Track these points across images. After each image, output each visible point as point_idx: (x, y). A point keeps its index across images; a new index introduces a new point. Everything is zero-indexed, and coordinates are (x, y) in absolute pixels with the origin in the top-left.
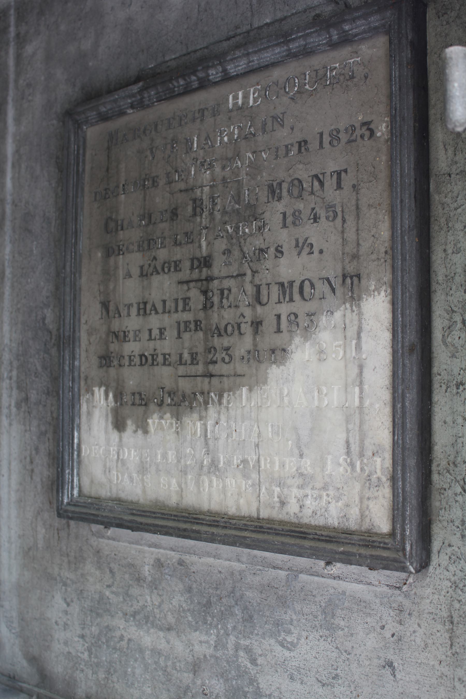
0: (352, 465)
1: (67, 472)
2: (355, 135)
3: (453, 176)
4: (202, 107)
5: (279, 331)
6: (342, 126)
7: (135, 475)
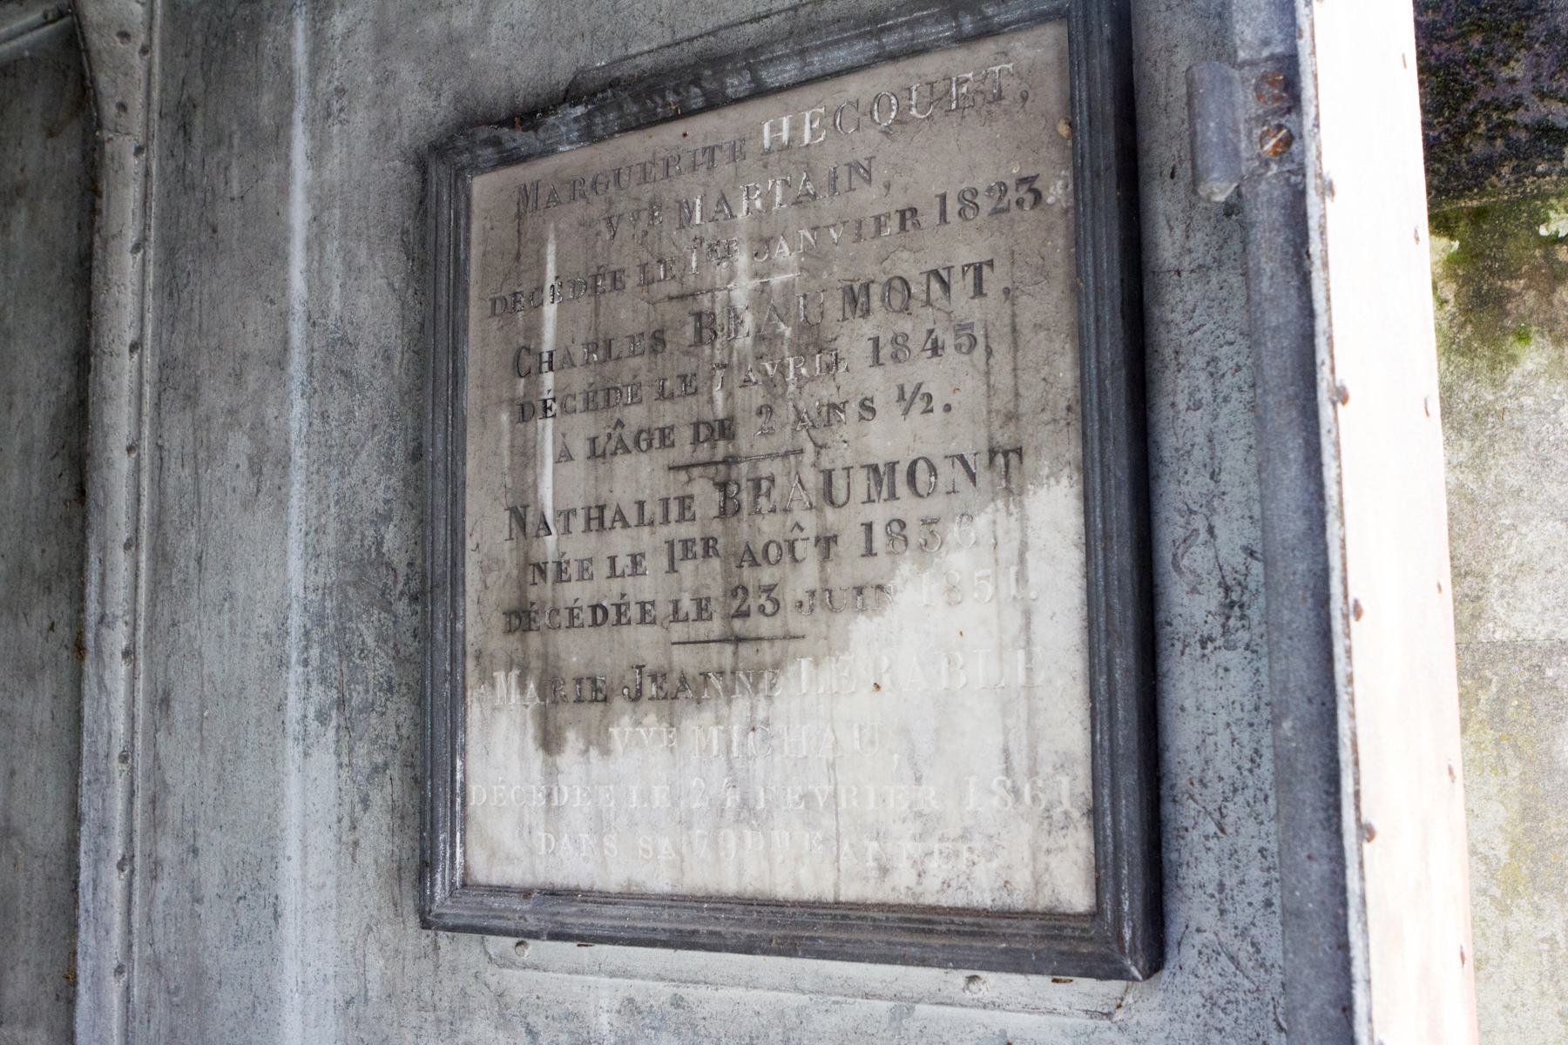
0: (1016, 792)
1: (441, 837)
2: (1005, 200)
3: (1184, 274)
4: (709, 143)
5: (870, 552)
6: (981, 184)
7: (584, 836)
